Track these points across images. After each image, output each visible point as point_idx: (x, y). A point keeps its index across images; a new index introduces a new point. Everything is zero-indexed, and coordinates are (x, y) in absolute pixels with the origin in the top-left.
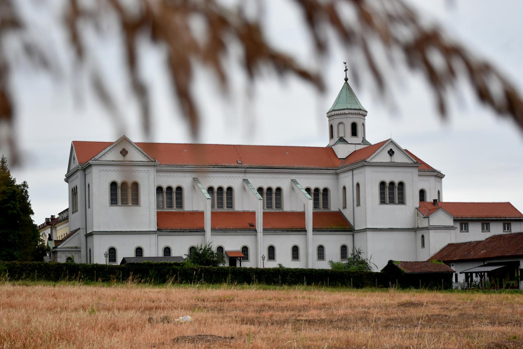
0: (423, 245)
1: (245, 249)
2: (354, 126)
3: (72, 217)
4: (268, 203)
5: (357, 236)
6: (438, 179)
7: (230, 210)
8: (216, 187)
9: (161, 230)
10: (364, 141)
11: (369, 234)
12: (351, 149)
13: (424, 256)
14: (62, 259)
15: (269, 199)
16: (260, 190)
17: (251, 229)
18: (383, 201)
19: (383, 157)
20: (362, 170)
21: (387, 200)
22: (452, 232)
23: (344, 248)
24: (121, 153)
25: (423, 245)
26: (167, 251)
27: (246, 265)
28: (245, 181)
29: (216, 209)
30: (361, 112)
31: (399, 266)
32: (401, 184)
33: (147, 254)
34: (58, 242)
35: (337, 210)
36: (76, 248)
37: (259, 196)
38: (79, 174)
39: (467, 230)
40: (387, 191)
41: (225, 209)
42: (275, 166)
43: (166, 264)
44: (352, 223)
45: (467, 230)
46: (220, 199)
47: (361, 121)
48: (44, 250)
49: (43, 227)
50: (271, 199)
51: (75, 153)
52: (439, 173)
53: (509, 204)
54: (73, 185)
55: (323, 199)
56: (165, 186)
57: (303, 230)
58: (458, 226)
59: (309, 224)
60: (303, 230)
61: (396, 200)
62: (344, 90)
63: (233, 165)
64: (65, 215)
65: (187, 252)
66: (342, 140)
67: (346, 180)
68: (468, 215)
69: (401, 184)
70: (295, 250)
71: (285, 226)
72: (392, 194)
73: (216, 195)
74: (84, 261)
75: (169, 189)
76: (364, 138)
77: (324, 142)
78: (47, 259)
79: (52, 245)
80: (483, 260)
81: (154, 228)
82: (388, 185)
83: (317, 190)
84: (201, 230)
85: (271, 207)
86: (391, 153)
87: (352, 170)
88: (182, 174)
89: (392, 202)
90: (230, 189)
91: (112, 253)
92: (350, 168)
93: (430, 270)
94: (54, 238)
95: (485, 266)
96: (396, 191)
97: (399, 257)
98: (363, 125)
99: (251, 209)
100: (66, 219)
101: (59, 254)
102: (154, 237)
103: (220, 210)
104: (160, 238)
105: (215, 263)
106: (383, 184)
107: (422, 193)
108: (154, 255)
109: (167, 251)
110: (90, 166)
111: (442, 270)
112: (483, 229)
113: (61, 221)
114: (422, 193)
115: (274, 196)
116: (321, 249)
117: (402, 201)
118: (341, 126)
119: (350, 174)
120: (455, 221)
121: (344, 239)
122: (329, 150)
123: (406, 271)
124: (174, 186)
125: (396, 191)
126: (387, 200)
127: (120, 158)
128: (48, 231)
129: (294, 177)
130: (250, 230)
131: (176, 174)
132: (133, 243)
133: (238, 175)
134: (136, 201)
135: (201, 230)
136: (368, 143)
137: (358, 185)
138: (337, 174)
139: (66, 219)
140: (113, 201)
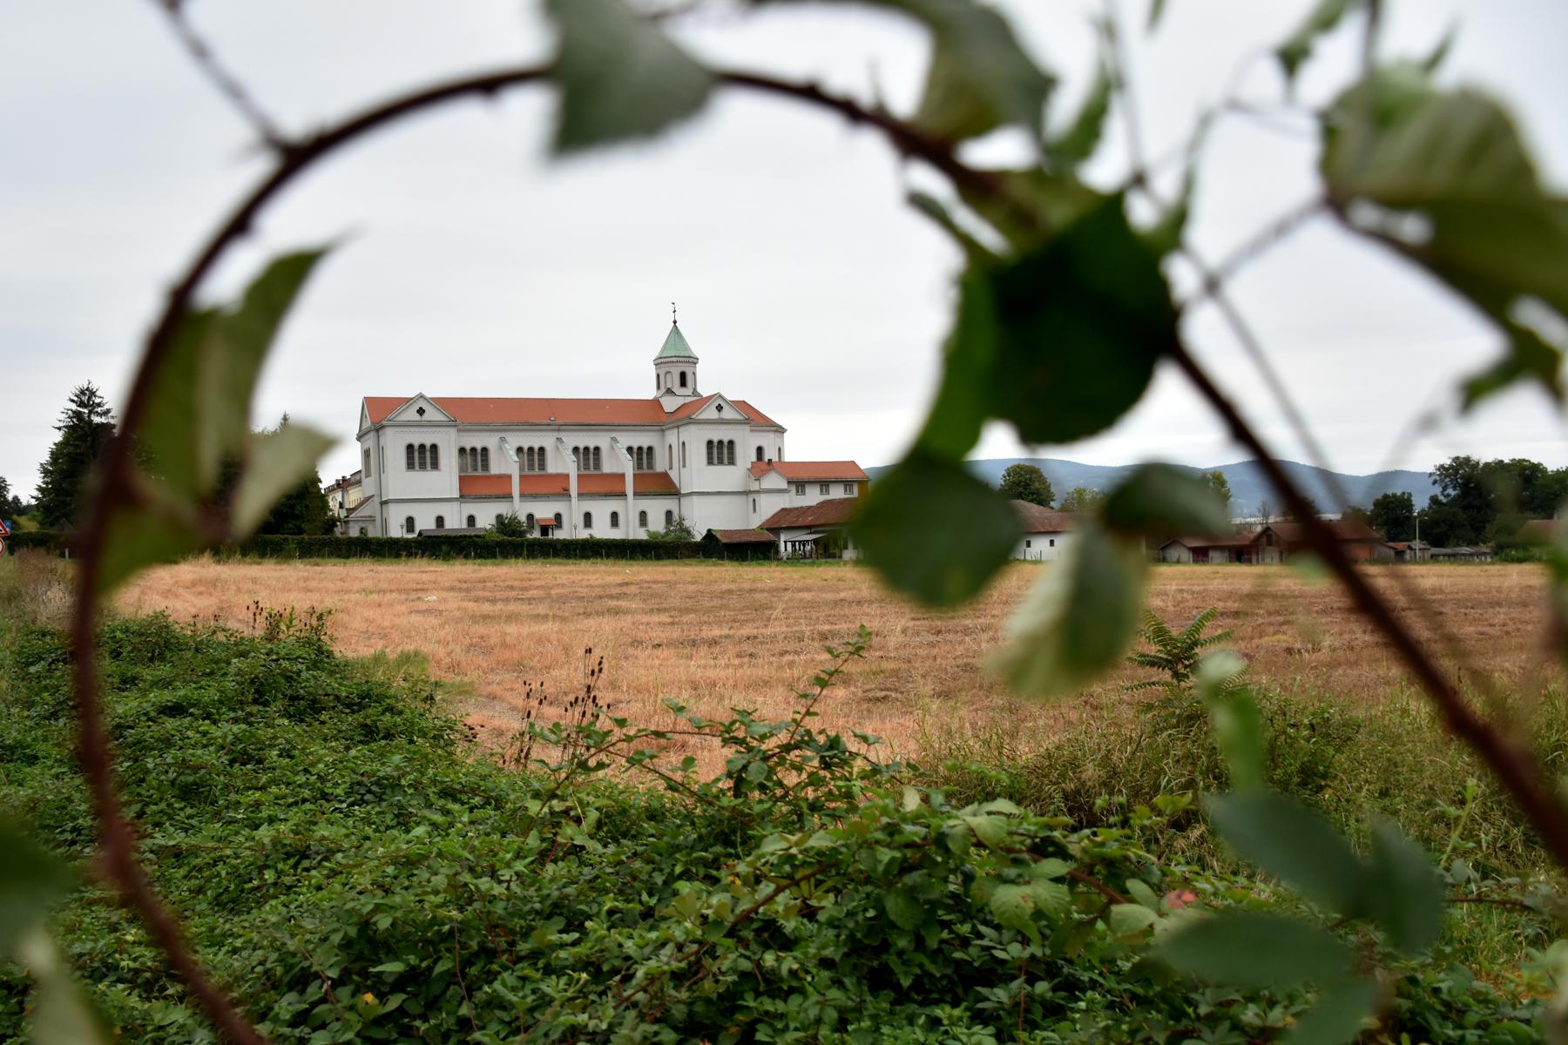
0: (755, 510)
1: (558, 517)
2: (683, 376)
3: (365, 481)
4: (638, 464)
5: (683, 500)
6: (779, 435)
7: (542, 473)
8: (526, 448)
9: (463, 497)
10: (695, 392)
11: (695, 499)
12: (680, 401)
13: (755, 521)
14: (354, 532)
15: (640, 459)
16: (630, 449)
17: (565, 494)
18: (710, 462)
19: (710, 413)
20: (687, 427)
21: (716, 460)
22: (786, 495)
23: (669, 514)
24: (418, 412)
25: (755, 510)
26: (471, 520)
27: (559, 535)
28: (559, 439)
29: (527, 472)
30: (691, 360)
31: (718, 535)
32: (731, 443)
33: (448, 525)
34: (350, 511)
35: (663, 470)
36: (370, 517)
37: (629, 457)
38: (372, 434)
39: (804, 493)
40: (715, 451)
41: (537, 471)
42: (593, 422)
43: (466, 536)
44: (678, 485)
45: (804, 493)
46: (531, 461)
47: (691, 370)
48: (333, 522)
49: (331, 489)
50: (533, 460)
51: (366, 411)
52: (781, 427)
53: (853, 463)
54: (366, 447)
55: (539, 460)
56: (468, 447)
57: (623, 495)
58: (793, 489)
59: (629, 488)
60: (623, 495)
61: (726, 461)
62: (672, 335)
63: (545, 422)
64: (357, 477)
65: (493, 521)
66: (669, 391)
67: (672, 437)
68: (804, 476)
69: (731, 443)
70: (614, 516)
71: (603, 490)
72: (720, 453)
73: (581, 456)
74: (379, 535)
75: (473, 450)
76: (695, 389)
77: (648, 392)
78: (338, 530)
79: (343, 514)
80: (808, 528)
81: (457, 495)
82: (716, 444)
83: (640, 449)
84: (508, 497)
85: (642, 468)
86: (720, 408)
87: (678, 427)
88: (488, 434)
89: (721, 462)
90: (542, 449)
91: (410, 522)
92: (676, 425)
93: (750, 539)
94: (347, 506)
95: (811, 533)
96: (725, 451)
97: (717, 526)
98: (694, 374)
99: (565, 472)
100: (359, 482)
101: (351, 524)
102: (456, 505)
103: (531, 473)
104: (463, 505)
105: (522, 534)
106: (710, 443)
107: (760, 450)
108: (457, 526)
109: (471, 520)
110: (383, 427)
111: (763, 539)
112: (821, 491)
113: (353, 484)
114: (760, 450)
115: (591, 456)
116: (643, 515)
117: (732, 462)
118: (669, 376)
119: (675, 431)
120: (789, 483)
121: (669, 504)
122: (656, 403)
123: (724, 540)
124: (479, 447)
125: (725, 451)
126: (716, 460)
127: (417, 417)
128: (338, 496)
129: (614, 435)
130: (563, 495)
131: (476, 434)
132: (433, 511)
133: (550, 434)
134: (435, 465)
135: (508, 497)
136: (699, 395)
137: (684, 443)
138: (663, 431)
139: (359, 482)
140: (410, 465)
